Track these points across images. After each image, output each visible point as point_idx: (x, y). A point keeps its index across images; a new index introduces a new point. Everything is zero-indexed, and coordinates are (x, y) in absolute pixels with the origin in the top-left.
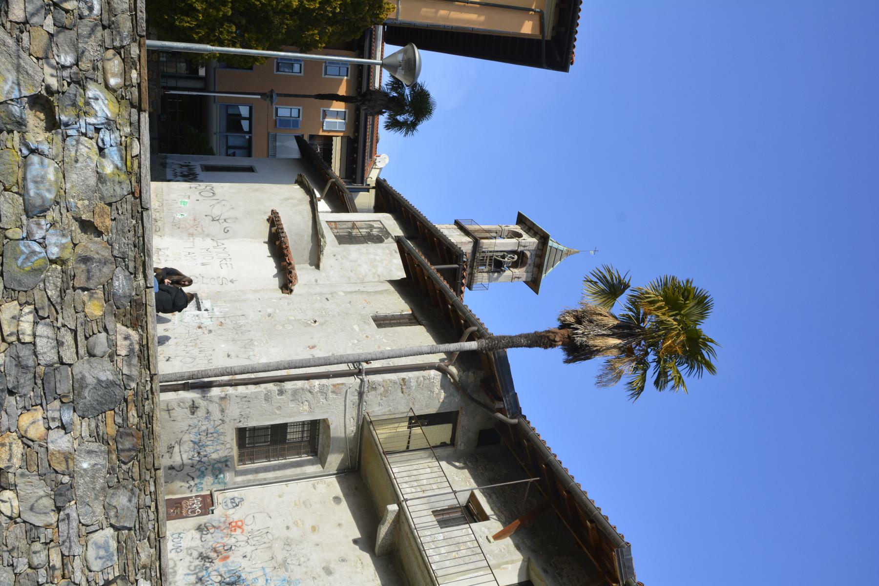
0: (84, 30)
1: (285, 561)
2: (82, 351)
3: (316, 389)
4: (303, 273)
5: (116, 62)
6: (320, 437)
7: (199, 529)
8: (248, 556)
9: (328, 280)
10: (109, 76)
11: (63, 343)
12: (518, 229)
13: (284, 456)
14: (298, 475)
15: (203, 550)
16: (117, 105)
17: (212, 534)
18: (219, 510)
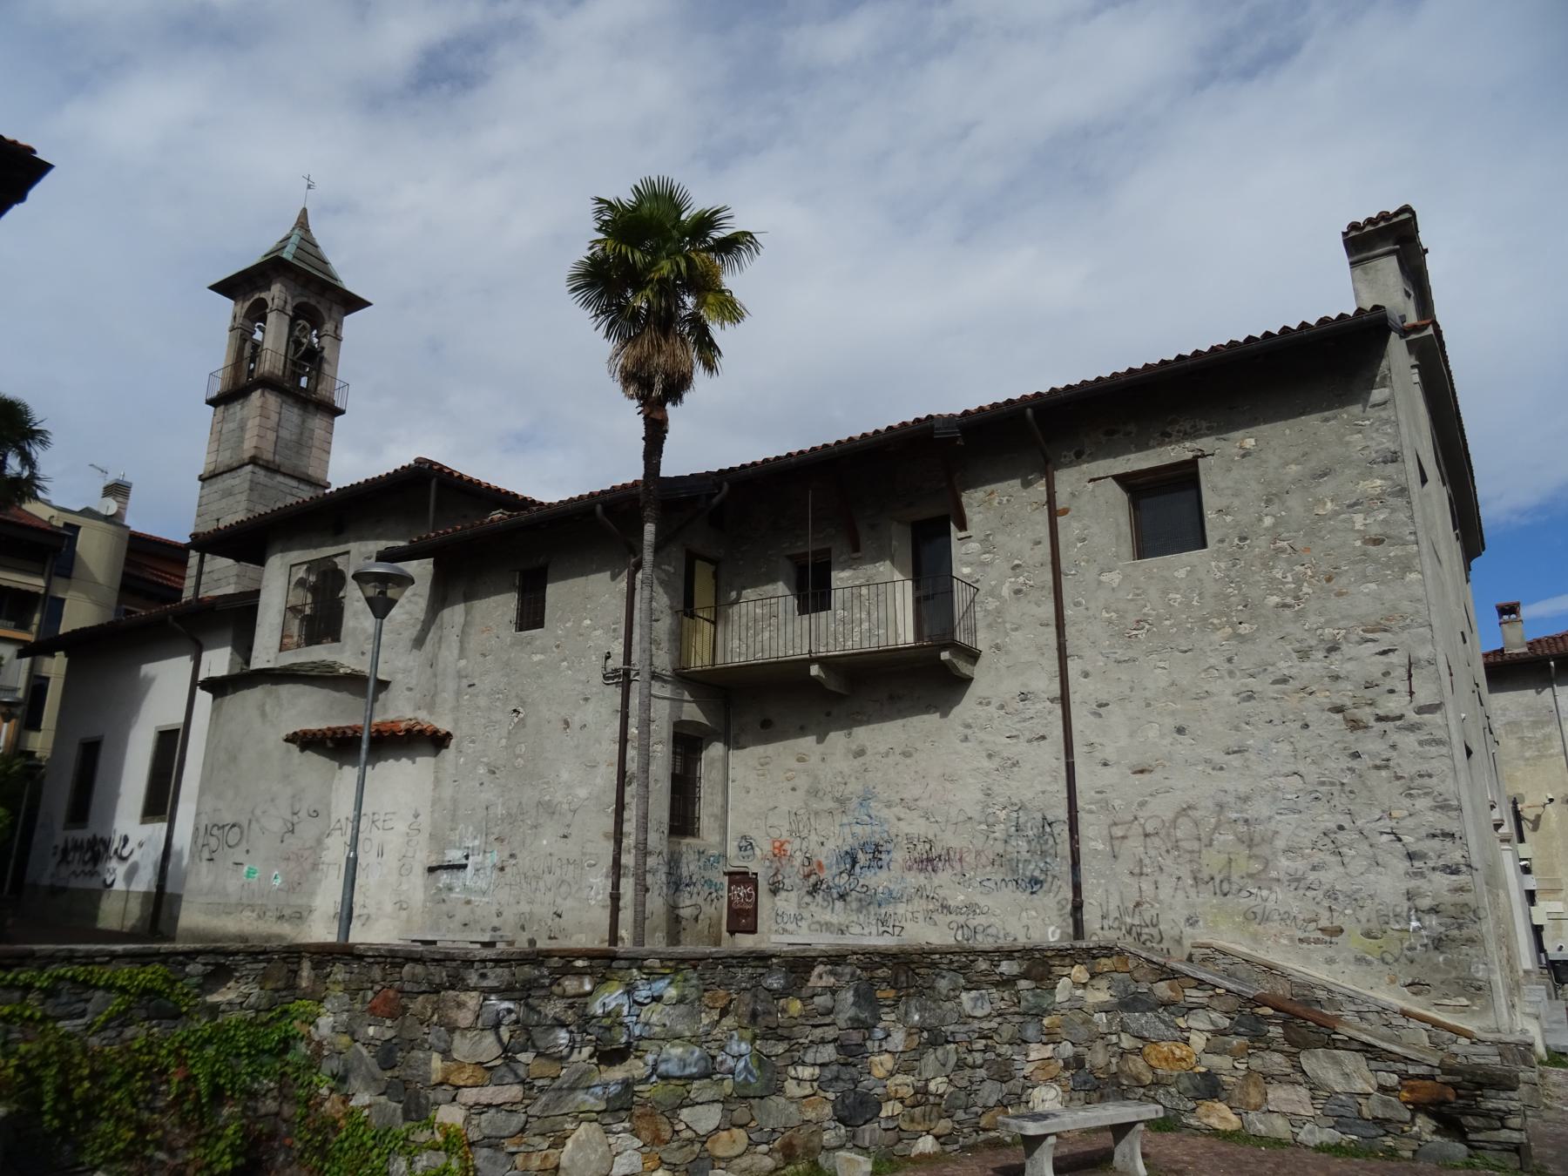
1: (837, 800)
4: (398, 710)
5: (567, 983)
6: (685, 732)
7: (775, 891)
8: (822, 839)
9: (410, 671)
10: (581, 991)
11: (822, 1038)
15: (805, 890)
16: (609, 983)
17: (784, 878)
18: (753, 867)
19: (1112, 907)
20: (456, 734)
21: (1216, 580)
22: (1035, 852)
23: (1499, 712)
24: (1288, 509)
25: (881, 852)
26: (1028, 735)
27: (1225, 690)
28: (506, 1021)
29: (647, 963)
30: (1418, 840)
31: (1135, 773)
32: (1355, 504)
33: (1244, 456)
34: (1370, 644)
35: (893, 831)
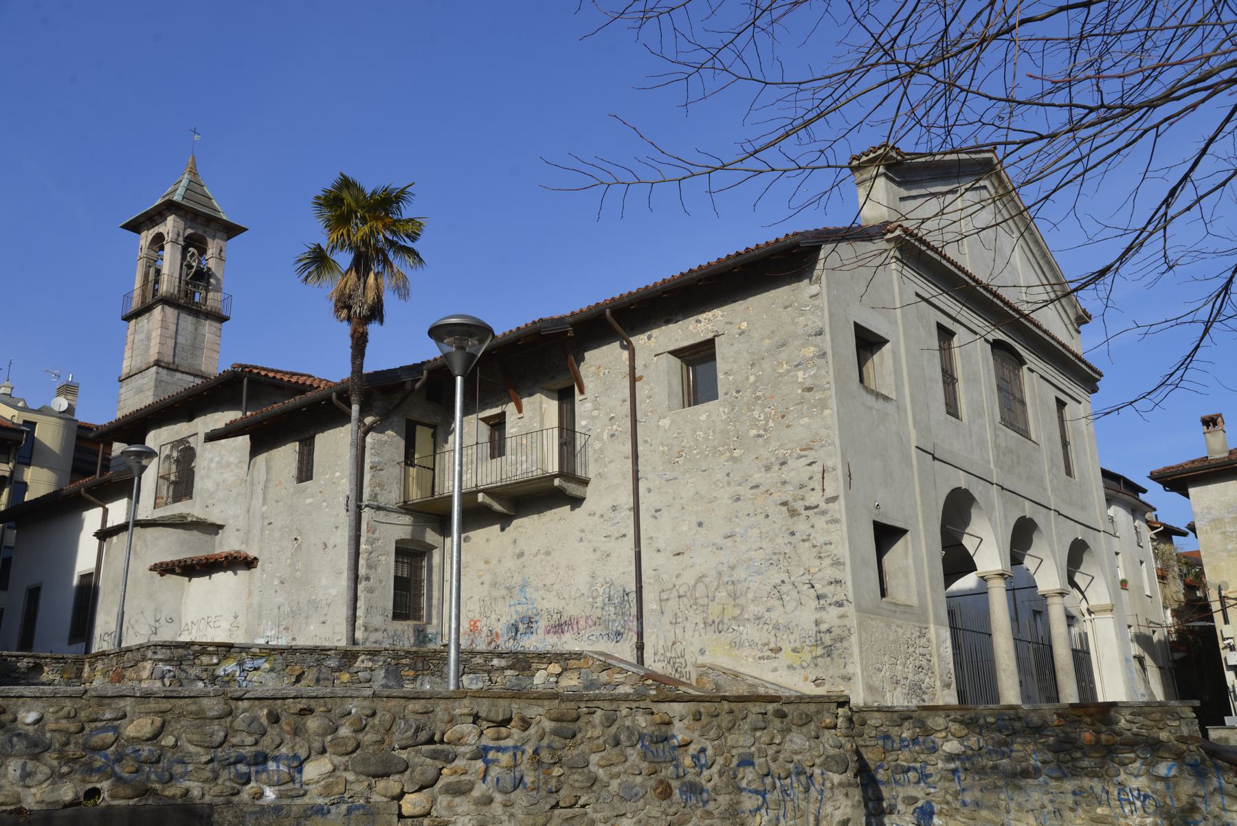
0: (183, 675)
2: (367, 685)
3: (369, 547)
4: (226, 544)
6: (410, 547)
8: (499, 617)
12: (147, 236)
13: (421, 581)
14: (440, 570)
19: (660, 647)
20: (261, 559)
21: (722, 421)
22: (618, 614)
23: (1205, 511)
24: (763, 370)
25: (532, 623)
26: (616, 535)
27: (724, 495)
28: (167, 676)
29: (253, 650)
30: (823, 586)
31: (675, 555)
32: (799, 365)
33: (740, 334)
34: (803, 459)
35: (539, 608)
